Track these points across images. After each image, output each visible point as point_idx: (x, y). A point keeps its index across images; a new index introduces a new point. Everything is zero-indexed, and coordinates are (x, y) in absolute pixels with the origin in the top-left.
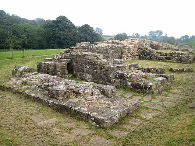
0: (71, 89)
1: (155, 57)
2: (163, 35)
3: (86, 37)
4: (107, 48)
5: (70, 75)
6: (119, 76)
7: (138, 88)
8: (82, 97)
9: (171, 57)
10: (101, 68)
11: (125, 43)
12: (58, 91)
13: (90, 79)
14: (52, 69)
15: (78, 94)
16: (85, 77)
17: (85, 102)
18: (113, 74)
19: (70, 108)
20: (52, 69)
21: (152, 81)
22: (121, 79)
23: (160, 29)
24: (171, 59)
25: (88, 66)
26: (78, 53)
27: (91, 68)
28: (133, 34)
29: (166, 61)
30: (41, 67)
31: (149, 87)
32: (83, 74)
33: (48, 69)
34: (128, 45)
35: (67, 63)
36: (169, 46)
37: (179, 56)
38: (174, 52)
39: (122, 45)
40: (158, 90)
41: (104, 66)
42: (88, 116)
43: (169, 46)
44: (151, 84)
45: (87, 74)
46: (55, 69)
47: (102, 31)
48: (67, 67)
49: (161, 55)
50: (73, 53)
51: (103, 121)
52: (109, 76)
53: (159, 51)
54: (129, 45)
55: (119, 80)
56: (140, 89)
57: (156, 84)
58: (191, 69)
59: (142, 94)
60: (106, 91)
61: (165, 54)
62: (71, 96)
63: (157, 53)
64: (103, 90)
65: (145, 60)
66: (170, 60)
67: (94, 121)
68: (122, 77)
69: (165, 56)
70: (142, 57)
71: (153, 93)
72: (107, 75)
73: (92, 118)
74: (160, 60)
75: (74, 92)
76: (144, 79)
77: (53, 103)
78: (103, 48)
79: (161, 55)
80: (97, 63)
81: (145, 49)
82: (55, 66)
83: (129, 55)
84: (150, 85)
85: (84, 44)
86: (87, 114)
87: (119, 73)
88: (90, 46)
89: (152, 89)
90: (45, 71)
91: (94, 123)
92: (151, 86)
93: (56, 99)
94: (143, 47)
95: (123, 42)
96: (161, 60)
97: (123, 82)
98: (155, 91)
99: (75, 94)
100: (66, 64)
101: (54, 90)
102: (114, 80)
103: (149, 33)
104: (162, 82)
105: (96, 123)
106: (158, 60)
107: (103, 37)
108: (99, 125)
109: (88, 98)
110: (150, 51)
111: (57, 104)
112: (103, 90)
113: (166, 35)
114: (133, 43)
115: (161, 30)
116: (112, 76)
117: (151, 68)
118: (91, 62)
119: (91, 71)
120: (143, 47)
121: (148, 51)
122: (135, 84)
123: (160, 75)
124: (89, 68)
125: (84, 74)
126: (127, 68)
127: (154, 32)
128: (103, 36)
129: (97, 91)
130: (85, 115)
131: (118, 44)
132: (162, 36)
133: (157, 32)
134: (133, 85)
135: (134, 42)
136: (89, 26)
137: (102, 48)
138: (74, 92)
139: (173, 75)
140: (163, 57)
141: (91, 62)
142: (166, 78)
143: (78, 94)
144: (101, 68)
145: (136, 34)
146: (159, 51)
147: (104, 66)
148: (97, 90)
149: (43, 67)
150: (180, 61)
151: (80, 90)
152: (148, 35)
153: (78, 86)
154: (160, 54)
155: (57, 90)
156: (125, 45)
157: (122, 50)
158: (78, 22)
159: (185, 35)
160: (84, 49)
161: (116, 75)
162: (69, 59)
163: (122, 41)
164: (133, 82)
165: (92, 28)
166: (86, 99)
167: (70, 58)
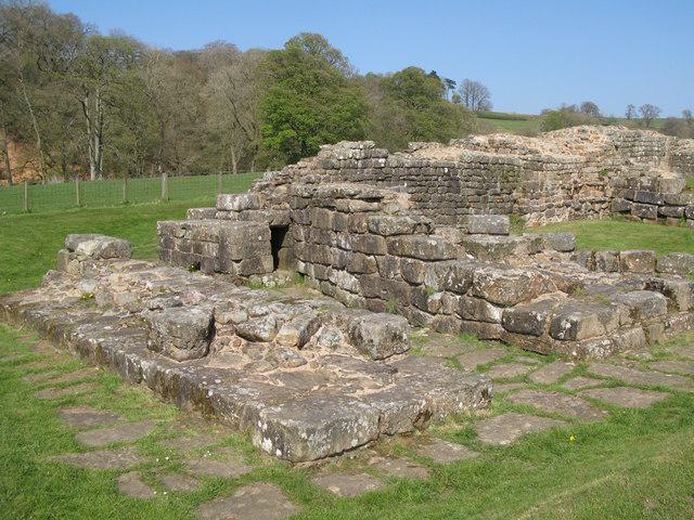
6: (456, 281)
8: (266, 351)
14: (211, 250)
17: (265, 371)
20: (211, 250)
28: (631, 107)
30: (173, 242)
31: (568, 326)
33: (198, 249)
34: (555, 156)
35: (272, 228)
46: (222, 248)
48: (269, 244)
54: (561, 156)
62: (225, 348)
67: (267, 435)
80: (377, 225)
81: (636, 174)
82: (221, 242)
83: (558, 199)
85: (346, 150)
89: (579, 335)
90: (184, 258)
92: (574, 324)
94: (627, 163)
97: (474, 307)
98: (590, 347)
99: (244, 342)
100: (265, 231)
102: (437, 296)
105: (274, 443)
108: (282, 449)
112: (354, 328)
118: (356, 223)
120: (627, 163)
121: (645, 182)
141: (356, 223)
142: (668, 293)
149: (178, 242)
156: (544, 155)
160: (345, 170)
167: (288, 206)
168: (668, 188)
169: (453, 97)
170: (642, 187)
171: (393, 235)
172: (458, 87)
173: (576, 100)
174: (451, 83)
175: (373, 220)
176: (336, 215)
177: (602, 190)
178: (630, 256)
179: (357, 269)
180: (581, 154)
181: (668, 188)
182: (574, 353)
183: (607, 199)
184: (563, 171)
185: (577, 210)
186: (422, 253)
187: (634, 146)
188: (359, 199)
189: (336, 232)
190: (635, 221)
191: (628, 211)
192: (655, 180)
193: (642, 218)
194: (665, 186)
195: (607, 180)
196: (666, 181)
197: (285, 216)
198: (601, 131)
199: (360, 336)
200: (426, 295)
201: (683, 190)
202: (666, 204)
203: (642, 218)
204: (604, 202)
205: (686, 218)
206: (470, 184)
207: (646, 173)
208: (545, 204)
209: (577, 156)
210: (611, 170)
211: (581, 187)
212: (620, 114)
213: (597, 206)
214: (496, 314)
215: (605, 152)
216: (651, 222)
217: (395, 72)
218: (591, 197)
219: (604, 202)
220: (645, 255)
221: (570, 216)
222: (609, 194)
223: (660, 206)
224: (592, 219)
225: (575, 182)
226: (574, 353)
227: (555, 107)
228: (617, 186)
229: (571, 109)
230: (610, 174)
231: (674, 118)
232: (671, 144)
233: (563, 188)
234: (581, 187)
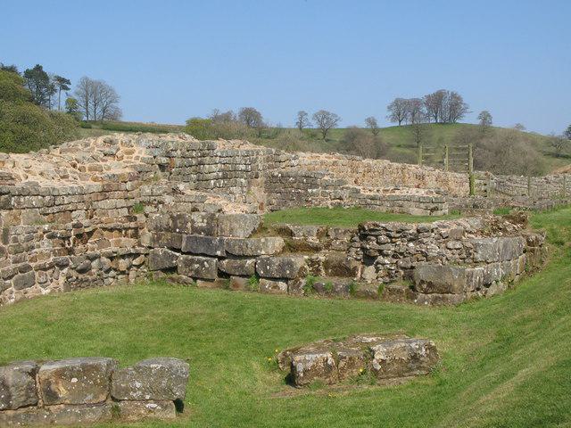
1: (249, 262)
2: (470, 118)
28: (302, 114)
36: (421, 177)
43: (421, 177)
54: (56, 184)
69: (317, 249)
70: (167, 265)
81: (184, 208)
94: (175, 191)
96: (286, 280)
103: (389, 108)
113: (485, 117)
115: (460, 93)
121: (199, 220)
127: (417, 103)
132: (464, 126)
133: (436, 101)
168: (232, 230)
169: (67, 102)
170: (195, 230)
172: (73, 87)
173: (234, 107)
174: (64, 83)
177: (136, 235)
178: (60, 374)
180: (95, 180)
181: (232, 230)
183: (142, 250)
184: (52, 205)
185: (82, 271)
187: (201, 163)
190: (185, 283)
191: (174, 269)
192: (212, 217)
193: (195, 279)
194: (226, 226)
195: (141, 218)
196: (229, 218)
198: (138, 142)
201: (254, 232)
202: (229, 255)
203: (195, 279)
204: (137, 255)
205: (258, 277)
207: (200, 207)
208: (11, 267)
209: (90, 182)
210: (149, 203)
211: (90, 234)
212: (289, 122)
213: (123, 264)
215: (140, 175)
216: (209, 285)
217: (528, 131)
218: (109, 250)
219: (137, 255)
220: (86, 370)
221: (68, 284)
222: (146, 241)
223: (221, 258)
224: (113, 286)
225: (78, 226)
227: (204, 114)
229: (227, 117)
230: (148, 209)
231: (355, 128)
232: (268, 160)
233: (52, 237)
234: (90, 234)
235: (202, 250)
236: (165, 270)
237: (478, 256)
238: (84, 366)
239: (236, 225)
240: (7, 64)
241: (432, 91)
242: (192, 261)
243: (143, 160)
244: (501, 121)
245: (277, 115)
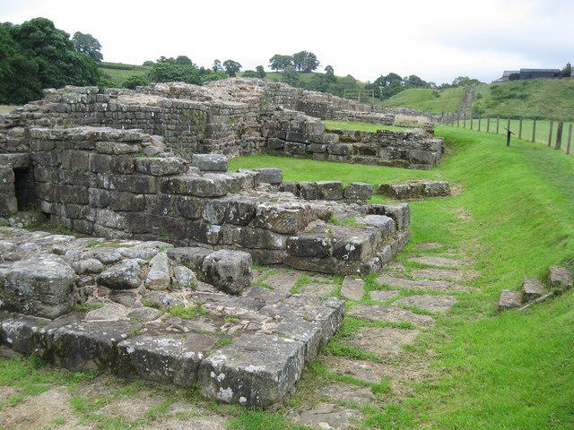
0: (87, 272)
2: (321, 70)
3: (42, 67)
4: (157, 113)
5: (28, 217)
6: (237, 215)
7: (313, 257)
9: (374, 145)
10: (166, 188)
11: (217, 93)
12: (45, 279)
13: (115, 228)
15: (118, 287)
16: (94, 222)
18: (216, 208)
19: (110, 344)
21: (355, 228)
22: (244, 224)
23: (309, 50)
24: (373, 153)
25: (109, 180)
26: (57, 128)
27: (121, 188)
28: (217, 61)
29: (358, 161)
31: (353, 248)
32: (87, 212)
37: (399, 142)
38: (383, 128)
39: (206, 102)
40: (377, 259)
41: (178, 178)
42: (198, 370)
44: (356, 240)
45: (102, 212)
47: (99, 46)
48: (12, 185)
49: (342, 140)
50: (36, 129)
51: (263, 378)
52: (197, 216)
53: (331, 125)
55: (239, 229)
56: (318, 260)
57: (372, 239)
58: (447, 185)
59: (331, 277)
60: (221, 271)
61: (353, 137)
62: (90, 298)
63: (327, 131)
64: (209, 268)
65: (287, 156)
66: (372, 158)
67: (225, 384)
68: (251, 216)
69: (355, 141)
70: (278, 146)
71: (366, 269)
72: (187, 213)
73: (218, 374)
74: (340, 158)
75: (101, 282)
76: (322, 223)
77: (25, 330)
78: (146, 112)
79: (342, 140)
80: (148, 167)
84: (355, 242)
86: (190, 360)
87: (236, 203)
88: (97, 104)
91: (227, 393)
92: (359, 247)
93: (34, 313)
94: (278, 109)
95: (206, 90)
96: (343, 155)
97: (257, 237)
98: (371, 263)
99: (108, 291)
100: (9, 173)
101: (21, 277)
102: (217, 229)
103: (271, 60)
104: (385, 231)
105: (235, 391)
106: (333, 157)
107: (105, 71)
108: (247, 395)
109: (164, 301)
110: (303, 124)
111: (45, 334)
112: (209, 268)
113: (329, 69)
114: (242, 96)
116: (208, 214)
117: (326, 186)
118: (123, 164)
119: (124, 197)
120: (278, 109)
122: (300, 241)
123: (366, 206)
124: (112, 187)
125: (92, 211)
126: (246, 184)
128: (102, 66)
129: (185, 274)
130: (184, 365)
131: (192, 97)
132: (317, 74)
134: (293, 246)
135: (244, 93)
136: (51, 25)
137: (140, 110)
138: (101, 282)
139: (407, 208)
140: (350, 146)
141: (123, 164)
143: (118, 287)
144: (166, 188)
145: (225, 63)
146: (331, 125)
147: (178, 178)
148: (183, 268)
150: (403, 159)
151: (129, 273)
152: (267, 69)
153: (113, 258)
154: (337, 136)
155: (39, 279)
156: (217, 101)
157: (208, 121)
158: (404, 73)
159: (391, 74)
160: (78, 114)
161: (227, 213)
162: (17, 151)
163: (202, 88)
164: (293, 233)
165: (63, 32)
166: (156, 306)
167: (26, 148)
170: (292, 129)
171: (166, 175)
175: (143, 162)
176: (96, 157)
177: (260, 131)
179: (123, 207)
180: (244, 102)
182: (358, 271)
186: (199, 191)
188: (123, 142)
189: (96, 173)
191: (283, 148)
194: (310, 128)
196: (312, 124)
197: (25, 159)
199: (217, 274)
200: (204, 230)
206: (169, 126)
214: (279, 241)
222: (266, 135)
223: (307, 144)
225: (243, 125)
226: (358, 271)
228: (271, 128)
235: (296, 140)
236: (277, 149)
237: (432, 148)
238: (335, 184)
239: (315, 128)
240: (18, 19)
241: (298, 51)
242: (292, 145)
243: (261, 92)
244: (340, 73)
245: (202, 61)
